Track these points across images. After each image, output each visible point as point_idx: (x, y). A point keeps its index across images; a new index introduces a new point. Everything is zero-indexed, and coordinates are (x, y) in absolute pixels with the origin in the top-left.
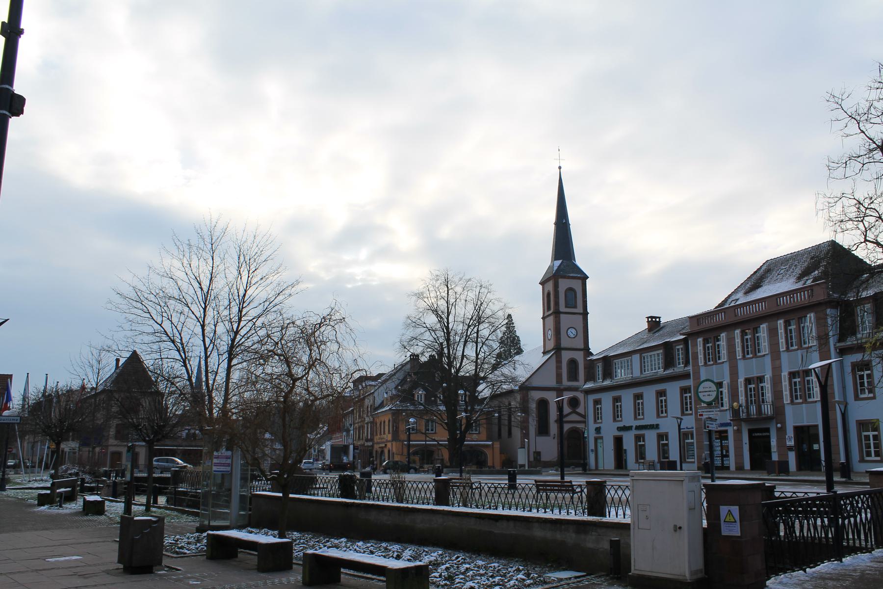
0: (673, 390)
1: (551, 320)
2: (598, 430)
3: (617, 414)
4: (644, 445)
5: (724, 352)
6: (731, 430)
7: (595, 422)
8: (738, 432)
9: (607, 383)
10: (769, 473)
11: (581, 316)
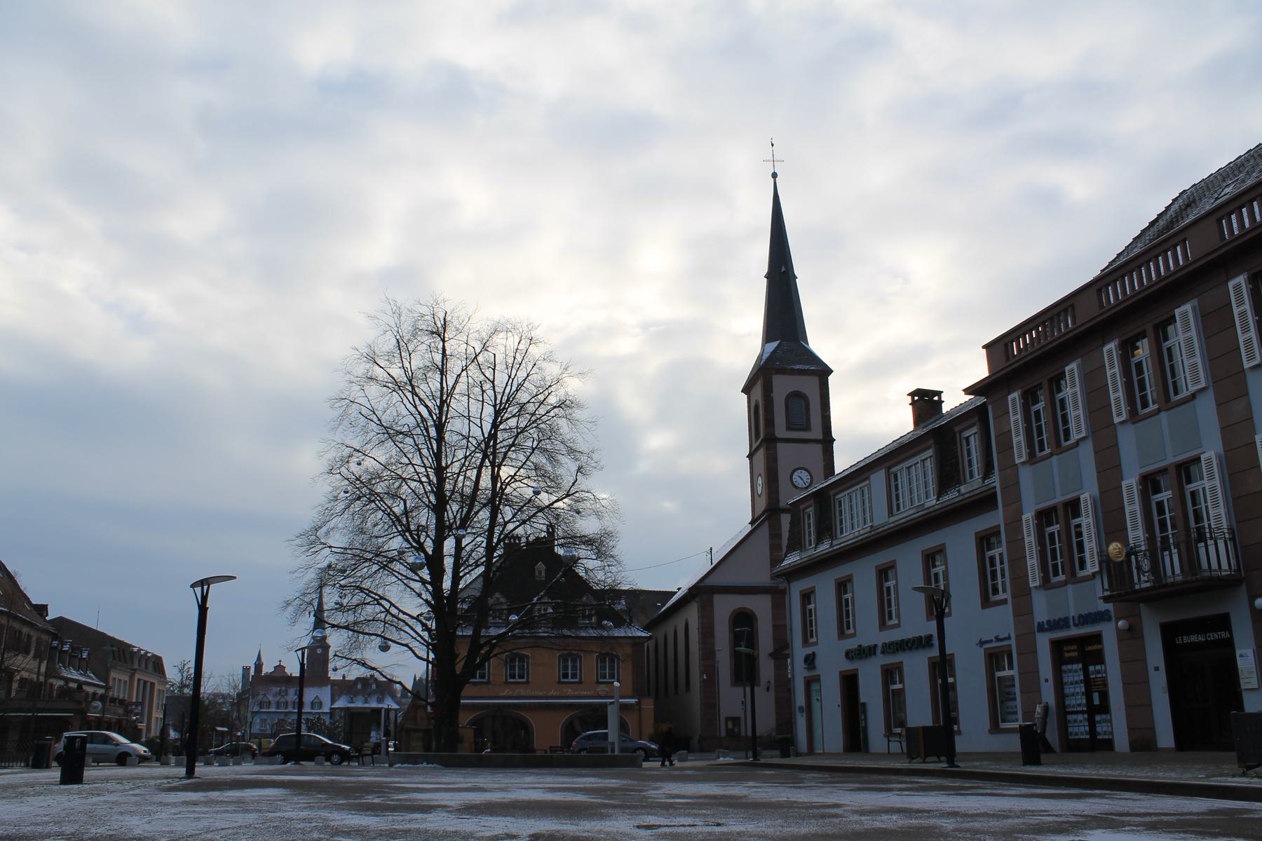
0: (959, 542)
1: (761, 454)
2: (810, 660)
3: (844, 625)
4: (902, 691)
5: (1077, 414)
6: (1109, 633)
7: (806, 642)
8: (1132, 635)
9: (825, 547)
10: (1247, 766)
11: (819, 447)
